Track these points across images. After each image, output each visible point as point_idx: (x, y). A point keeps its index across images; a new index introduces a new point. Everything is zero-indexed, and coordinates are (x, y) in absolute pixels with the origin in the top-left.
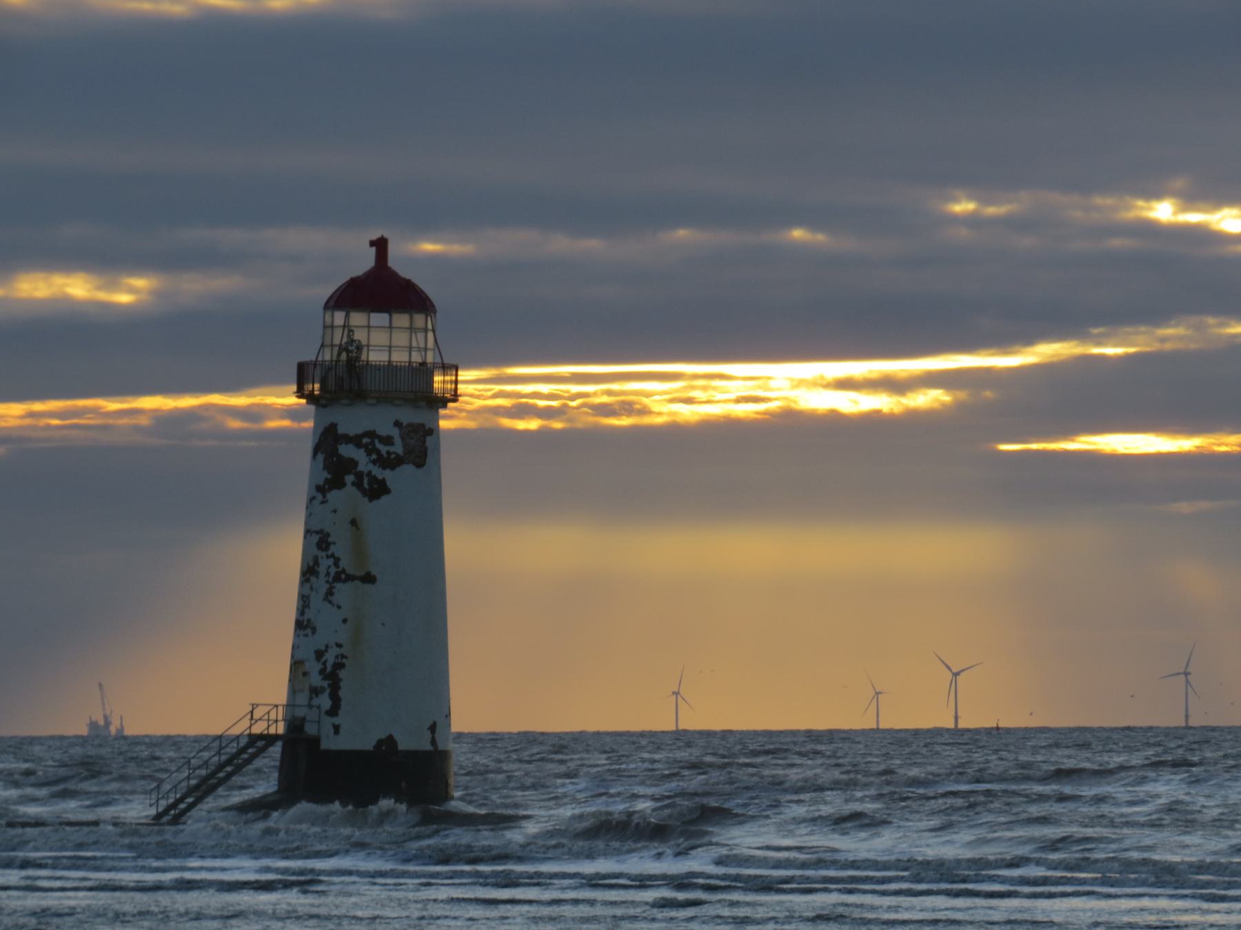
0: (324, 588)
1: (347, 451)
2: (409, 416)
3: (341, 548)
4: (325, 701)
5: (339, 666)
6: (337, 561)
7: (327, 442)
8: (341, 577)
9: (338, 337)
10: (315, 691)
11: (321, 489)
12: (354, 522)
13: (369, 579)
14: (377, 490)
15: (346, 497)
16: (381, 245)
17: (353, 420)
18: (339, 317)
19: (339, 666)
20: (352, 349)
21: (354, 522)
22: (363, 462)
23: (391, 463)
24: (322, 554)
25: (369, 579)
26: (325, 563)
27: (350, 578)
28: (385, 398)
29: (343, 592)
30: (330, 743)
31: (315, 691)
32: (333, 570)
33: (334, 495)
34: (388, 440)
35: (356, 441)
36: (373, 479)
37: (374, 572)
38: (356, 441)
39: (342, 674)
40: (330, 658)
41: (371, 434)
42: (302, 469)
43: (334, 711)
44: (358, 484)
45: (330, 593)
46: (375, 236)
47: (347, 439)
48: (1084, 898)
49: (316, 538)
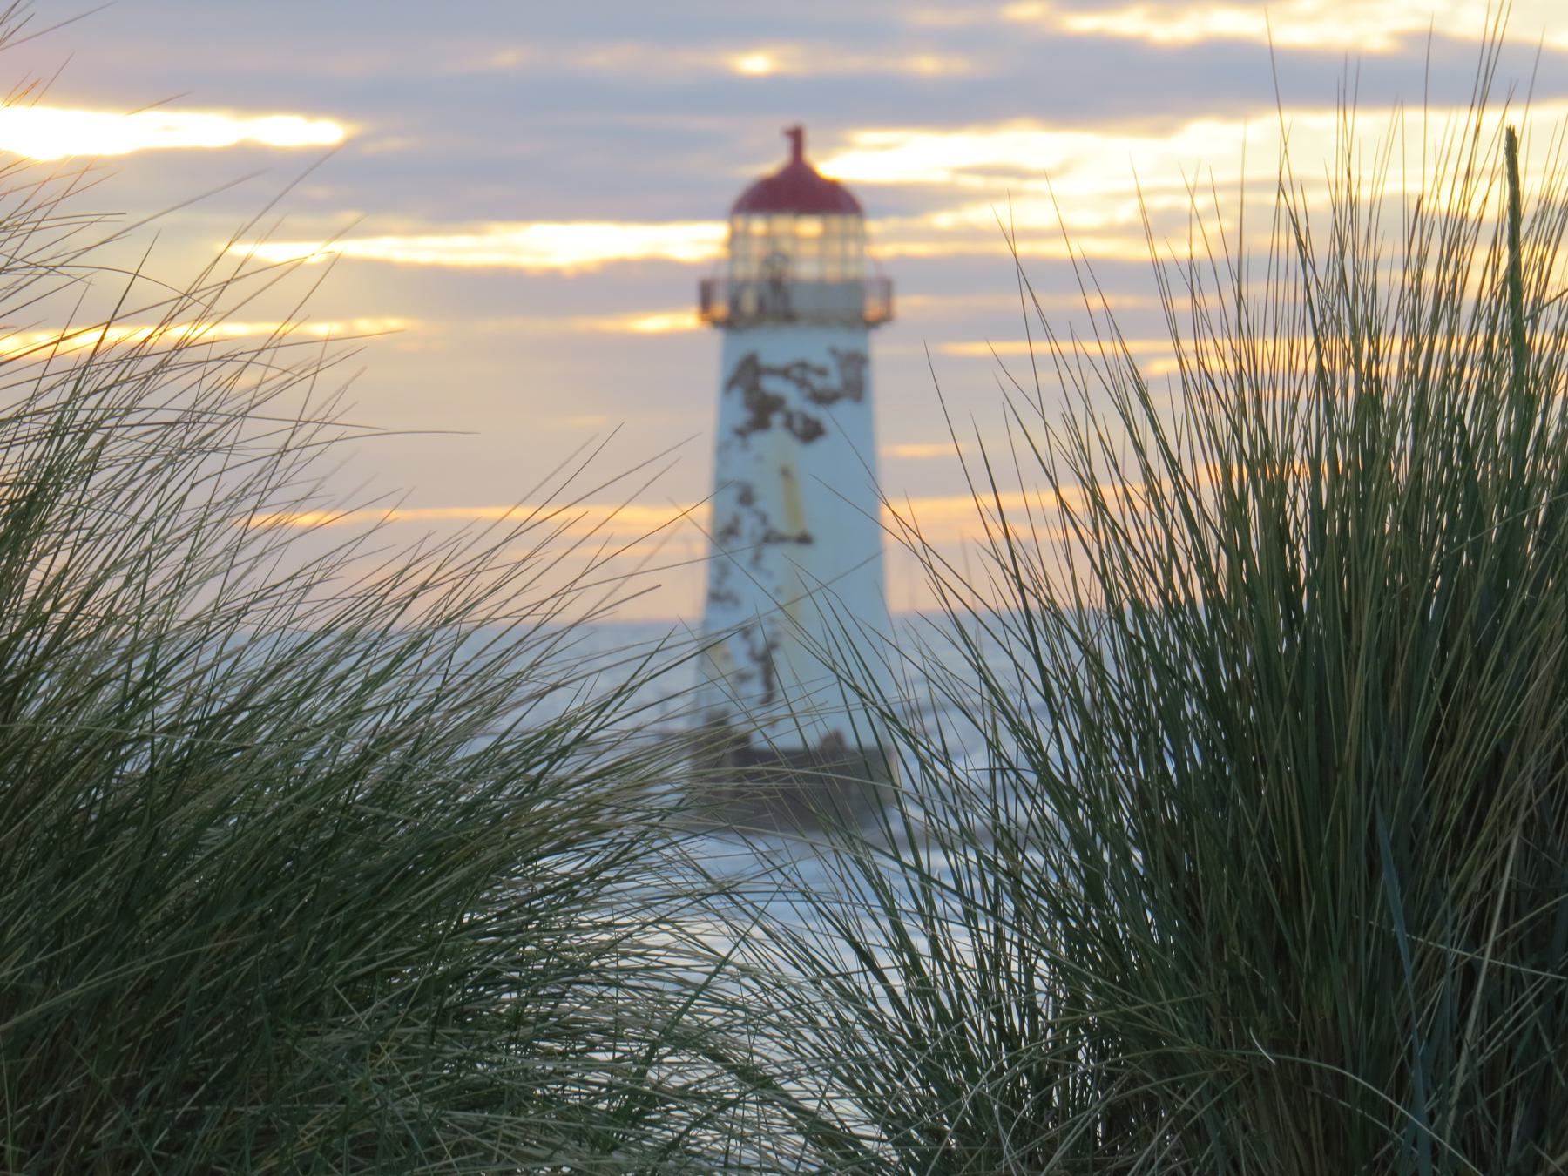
0: (748, 554)
1: (772, 385)
2: (845, 341)
3: (770, 499)
4: (756, 689)
5: (772, 646)
6: (764, 519)
7: (746, 377)
8: (771, 538)
9: (757, 250)
10: (743, 678)
11: (741, 433)
12: (785, 473)
13: (805, 540)
14: (811, 432)
15: (776, 441)
16: (796, 137)
17: (777, 347)
18: (758, 226)
19: (772, 646)
20: (776, 260)
21: (785, 473)
22: (794, 398)
23: (824, 398)
24: (744, 512)
25: (805, 540)
26: (749, 524)
27: (782, 539)
28: (821, 320)
29: (774, 556)
30: (786, 738)
31: (743, 678)
32: (760, 531)
33: (759, 440)
34: (822, 372)
35: (785, 373)
36: (807, 421)
37: (812, 530)
38: (785, 373)
39: (777, 656)
40: (760, 640)
41: (803, 365)
42: (699, 411)
43: (768, 700)
44: (789, 424)
45: (757, 559)
46: (790, 122)
47: (772, 371)
48: (1506, 169)
49: (733, 493)
